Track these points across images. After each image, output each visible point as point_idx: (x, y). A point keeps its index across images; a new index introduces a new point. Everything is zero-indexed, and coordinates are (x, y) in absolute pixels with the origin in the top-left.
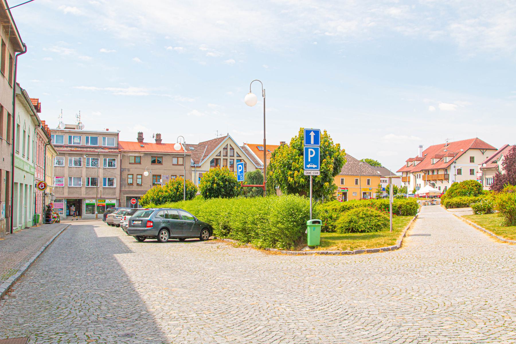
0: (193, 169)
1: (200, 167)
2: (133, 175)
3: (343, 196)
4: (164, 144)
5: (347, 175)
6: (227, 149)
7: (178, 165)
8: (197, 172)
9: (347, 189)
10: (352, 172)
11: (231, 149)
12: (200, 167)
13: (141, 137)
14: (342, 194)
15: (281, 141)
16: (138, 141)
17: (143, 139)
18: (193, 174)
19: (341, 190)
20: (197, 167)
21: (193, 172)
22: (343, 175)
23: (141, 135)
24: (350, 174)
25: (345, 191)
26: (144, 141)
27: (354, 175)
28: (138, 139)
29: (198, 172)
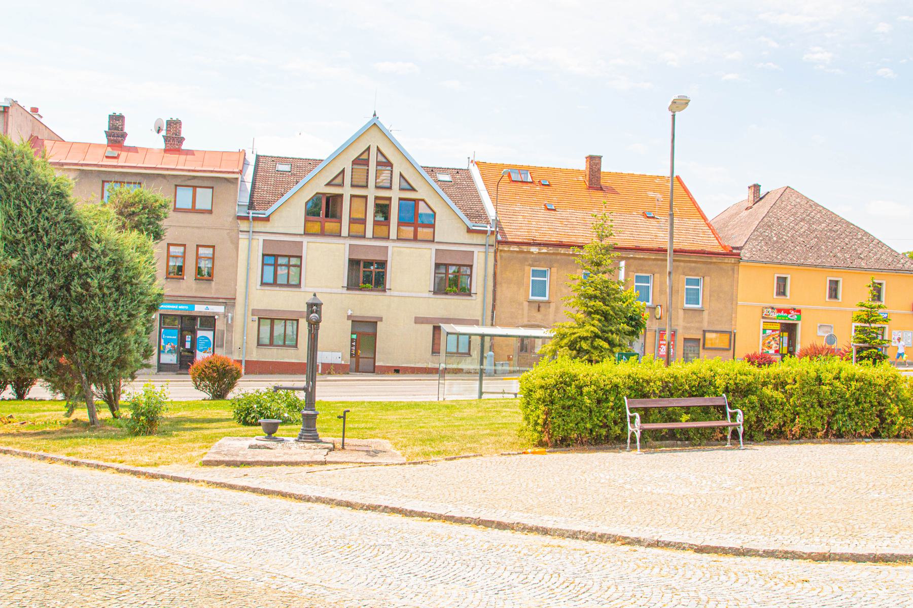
0: (244, 226)
1: (267, 219)
2: (213, 247)
3: (786, 334)
4: (190, 152)
5: (799, 265)
6: (366, 162)
7: (194, 210)
8: (256, 236)
9: (799, 311)
10: (819, 257)
11: (379, 164)
12: (267, 219)
13: (117, 128)
14: (778, 327)
15: (587, 155)
16: (109, 140)
17: (124, 136)
18: (243, 243)
19: (775, 315)
20: (255, 219)
21: (241, 236)
22: (785, 264)
23: (118, 123)
24: (809, 262)
25: (790, 319)
26: (128, 142)
27: (823, 267)
28: (107, 136)
29: (262, 238)
